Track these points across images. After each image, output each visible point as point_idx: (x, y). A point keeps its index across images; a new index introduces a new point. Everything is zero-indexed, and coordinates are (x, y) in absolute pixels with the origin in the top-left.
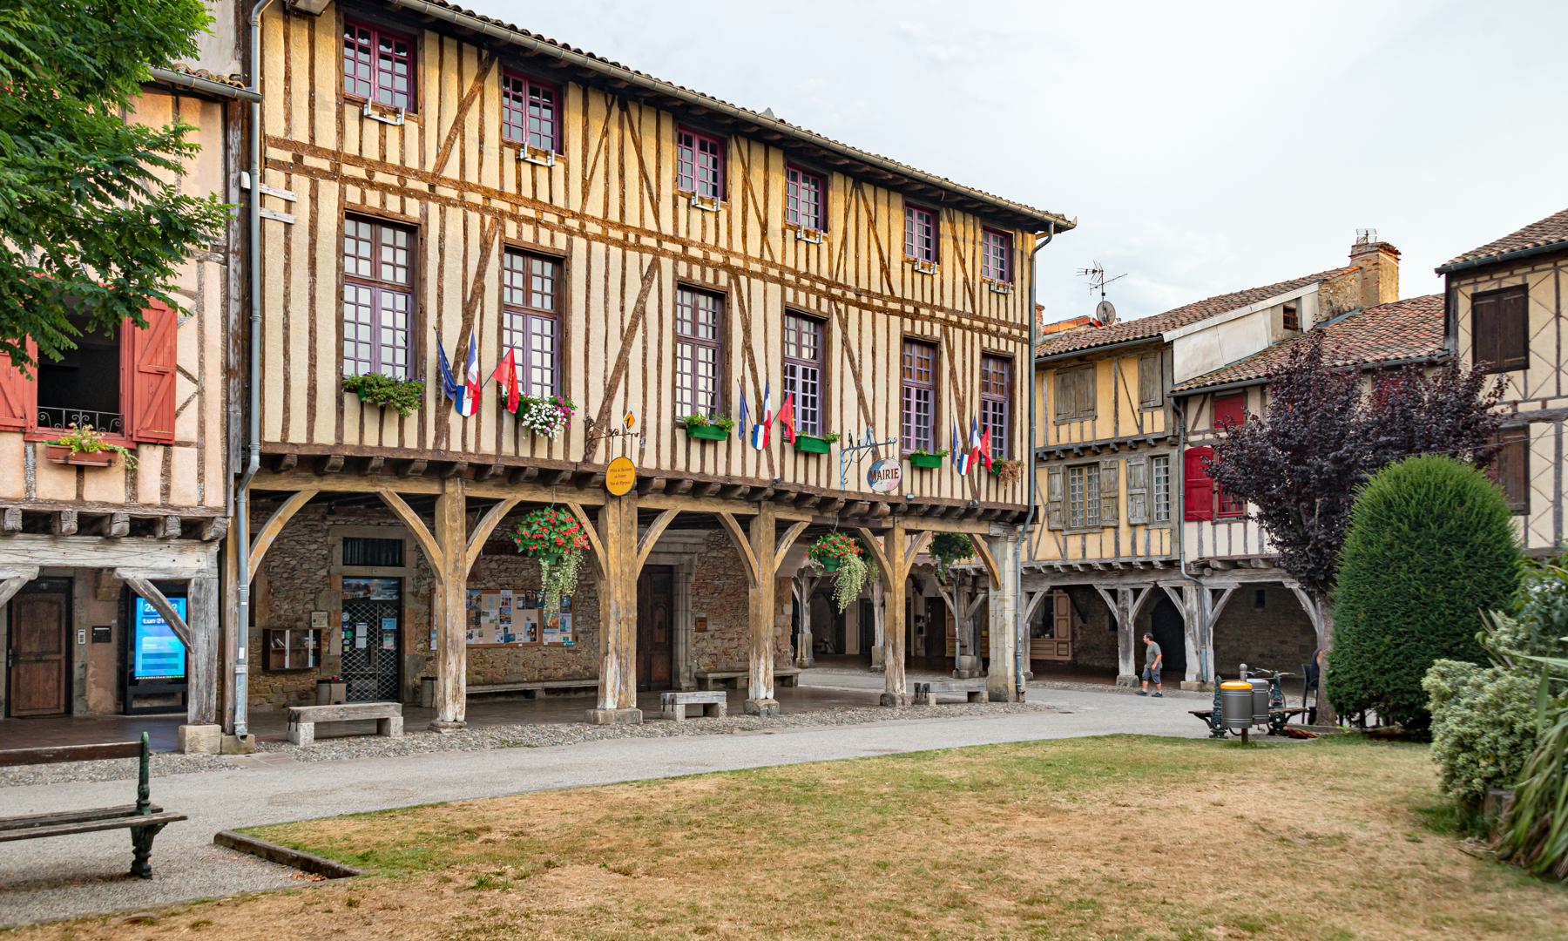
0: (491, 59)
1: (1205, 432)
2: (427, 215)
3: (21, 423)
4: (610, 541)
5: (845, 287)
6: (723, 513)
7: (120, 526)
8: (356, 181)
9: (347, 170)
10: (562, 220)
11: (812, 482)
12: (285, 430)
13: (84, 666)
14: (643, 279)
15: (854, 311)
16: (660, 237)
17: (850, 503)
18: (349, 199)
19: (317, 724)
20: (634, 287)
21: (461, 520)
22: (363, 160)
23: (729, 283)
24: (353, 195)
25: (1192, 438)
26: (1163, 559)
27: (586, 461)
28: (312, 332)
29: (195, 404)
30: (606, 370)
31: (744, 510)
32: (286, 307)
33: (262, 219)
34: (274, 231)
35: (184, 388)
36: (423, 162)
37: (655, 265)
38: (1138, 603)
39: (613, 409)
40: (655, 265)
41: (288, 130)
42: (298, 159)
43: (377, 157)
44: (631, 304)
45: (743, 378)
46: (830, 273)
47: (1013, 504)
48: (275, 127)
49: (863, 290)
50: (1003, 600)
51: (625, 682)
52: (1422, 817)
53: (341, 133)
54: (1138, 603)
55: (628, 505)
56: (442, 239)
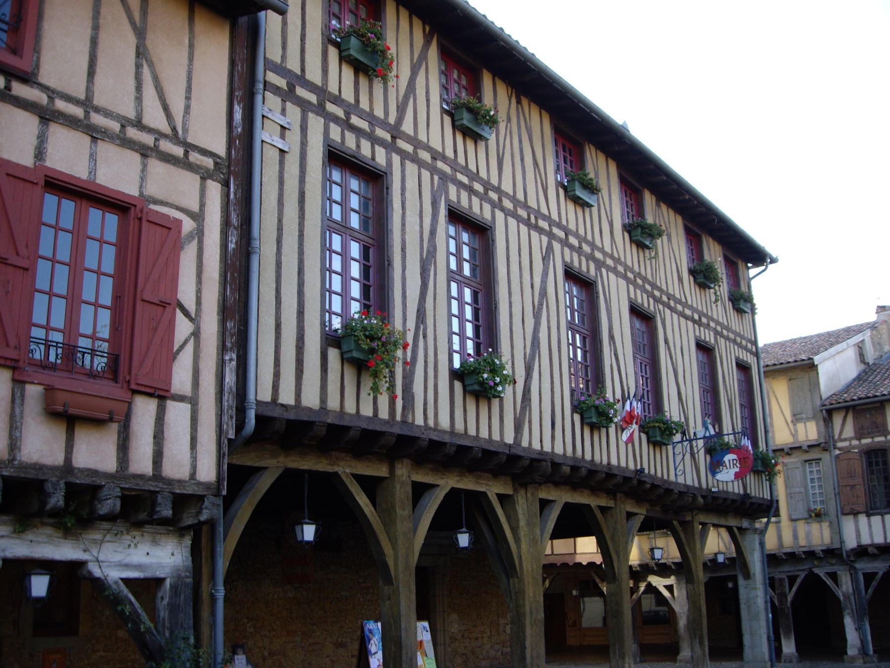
1: (850, 439)
3: (12, 354)
6: (593, 506)
7: (110, 504)
8: (336, 119)
9: (330, 107)
14: (543, 259)
22: (343, 101)
24: (335, 132)
25: (840, 444)
26: (824, 548)
29: (190, 347)
30: (525, 347)
31: (604, 502)
35: (183, 327)
36: (386, 113)
37: (550, 248)
38: (794, 589)
40: (550, 248)
41: (284, 57)
42: (291, 88)
45: (611, 365)
50: (755, 589)
54: (794, 589)
55: (532, 494)
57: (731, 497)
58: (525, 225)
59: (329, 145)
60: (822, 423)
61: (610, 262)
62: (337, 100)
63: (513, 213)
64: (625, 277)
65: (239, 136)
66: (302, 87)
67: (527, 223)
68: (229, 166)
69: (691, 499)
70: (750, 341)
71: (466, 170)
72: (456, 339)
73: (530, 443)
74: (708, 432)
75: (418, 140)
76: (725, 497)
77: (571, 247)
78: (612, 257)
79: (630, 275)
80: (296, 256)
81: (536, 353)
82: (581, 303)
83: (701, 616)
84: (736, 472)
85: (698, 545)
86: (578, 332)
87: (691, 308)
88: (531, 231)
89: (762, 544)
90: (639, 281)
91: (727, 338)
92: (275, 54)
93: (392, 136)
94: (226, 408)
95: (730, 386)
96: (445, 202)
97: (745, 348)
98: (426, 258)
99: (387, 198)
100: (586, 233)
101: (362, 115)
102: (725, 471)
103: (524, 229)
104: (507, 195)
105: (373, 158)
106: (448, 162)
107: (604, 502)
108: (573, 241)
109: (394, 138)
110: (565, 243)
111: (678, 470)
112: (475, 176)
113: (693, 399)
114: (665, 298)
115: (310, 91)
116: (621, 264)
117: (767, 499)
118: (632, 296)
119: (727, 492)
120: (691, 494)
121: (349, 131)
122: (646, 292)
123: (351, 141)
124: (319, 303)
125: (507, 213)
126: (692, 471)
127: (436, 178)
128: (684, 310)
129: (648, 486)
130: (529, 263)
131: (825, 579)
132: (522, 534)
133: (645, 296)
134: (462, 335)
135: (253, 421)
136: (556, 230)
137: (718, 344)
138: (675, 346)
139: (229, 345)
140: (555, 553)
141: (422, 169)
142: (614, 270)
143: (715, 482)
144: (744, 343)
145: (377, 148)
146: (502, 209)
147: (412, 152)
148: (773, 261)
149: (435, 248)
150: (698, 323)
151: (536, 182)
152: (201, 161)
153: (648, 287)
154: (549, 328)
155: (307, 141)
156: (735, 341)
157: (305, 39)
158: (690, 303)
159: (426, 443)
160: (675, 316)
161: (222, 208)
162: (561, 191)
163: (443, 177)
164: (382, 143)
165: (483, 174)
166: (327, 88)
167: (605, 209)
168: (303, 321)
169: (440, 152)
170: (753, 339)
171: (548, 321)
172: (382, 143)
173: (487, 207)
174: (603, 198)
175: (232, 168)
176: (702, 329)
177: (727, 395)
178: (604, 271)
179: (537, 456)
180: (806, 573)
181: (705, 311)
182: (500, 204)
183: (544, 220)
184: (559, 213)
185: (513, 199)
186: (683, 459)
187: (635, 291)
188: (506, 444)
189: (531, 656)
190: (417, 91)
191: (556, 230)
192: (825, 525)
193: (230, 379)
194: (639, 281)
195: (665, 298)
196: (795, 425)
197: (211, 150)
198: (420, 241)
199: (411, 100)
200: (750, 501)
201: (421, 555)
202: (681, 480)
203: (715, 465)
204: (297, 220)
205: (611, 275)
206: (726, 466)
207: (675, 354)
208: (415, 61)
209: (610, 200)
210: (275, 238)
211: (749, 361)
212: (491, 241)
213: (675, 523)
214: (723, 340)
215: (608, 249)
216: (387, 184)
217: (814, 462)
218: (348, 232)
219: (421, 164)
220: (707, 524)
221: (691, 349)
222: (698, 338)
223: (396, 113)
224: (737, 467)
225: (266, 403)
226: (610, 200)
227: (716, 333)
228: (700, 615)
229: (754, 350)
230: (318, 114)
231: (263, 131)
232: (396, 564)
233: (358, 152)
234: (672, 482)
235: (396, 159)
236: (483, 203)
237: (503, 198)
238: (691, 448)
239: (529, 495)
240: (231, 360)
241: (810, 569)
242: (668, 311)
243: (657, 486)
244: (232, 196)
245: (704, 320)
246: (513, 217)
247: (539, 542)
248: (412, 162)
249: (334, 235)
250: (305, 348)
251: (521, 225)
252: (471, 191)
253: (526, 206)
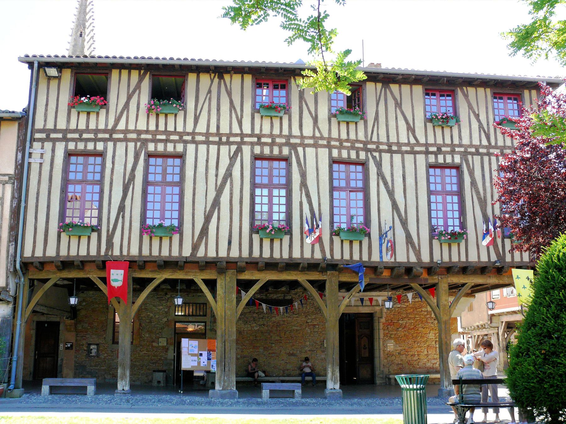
0: (145, 74)
4: (218, 298)
5: (378, 143)
10: (477, 150)
11: (356, 257)
13: (62, 360)
15: (386, 157)
16: (242, 135)
30: (205, 208)
34: (35, 168)
37: (239, 150)
39: (210, 227)
43: (478, 144)
44: (222, 171)
45: (301, 203)
46: (366, 136)
47: (324, 259)
48: (39, 124)
49: (392, 143)
56: (114, 157)
65: (19, 165)
98: (128, 183)
168: (48, 225)
208: (130, 93)
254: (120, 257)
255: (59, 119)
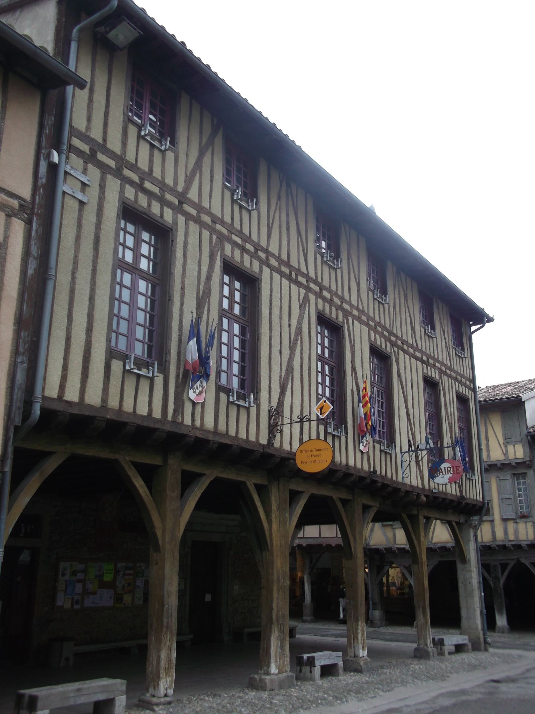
2: (186, 224)
6: (334, 497)
8: (132, 183)
9: (127, 172)
12: (62, 387)
14: (300, 306)
17: (407, 492)
18: (127, 195)
19: (51, 711)
20: (296, 310)
21: (177, 492)
22: (138, 169)
23: (344, 320)
24: (130, 193)
26: (529, 543)
27: (270, 443)
28: (92, 299)
30: (281, 372)
31: (344, 495)
32: (73, 273)
33: (64, 193)
36: (176, 182)
37: (306, 298)
40: (306, 298)
41: (88, 128)
44: (294, 322)
45: (352, 390)
51: (282, 647)
52: (157, 688)
53: (124, 143)
54: (506, 574)
57: (449, 497)
58: (287, 279)
59: (123, 202)
60: (527, 445)
61: (355, 312)
62: (134, 167)
63: (278, 269)
64: (367, 325)
66: (103, 153)
67: (289, 278)
68: (33, 209)
69: (415, 497)
70: (469, 380)
71: (240, 233)
72: (224, 362)
73: (281, 445)
74: (428, 445)
75: (202, 206)
76: (445, 497)
77: (324, 299)
78: (357, 309)
79: (371, 323)
80: (88, 285)
81: (289, 376)
82: (331, 342)
83: (424, 590)
84: (450, 477)
85: (422, 534)
86: (327, 364)
87: (421, 351)
88: (292, 284)
89: (476, 537)
90: (379, 329)
91: (450, 376)
92: (80, 123)
93: (179, 202)
94: (15, 400)
95: (451, 412)
96: (221, 256)
97: (465, 385)
98: (202, 297)
99: (172, 249)
100: (337, 289)
101: (154, 181)
102: (441, 475)
103: (285, 282)
104: (273, 255)
105: (162, 216)
106: (225, 226)
107: (344, 495)
108: (325, 294)
109: (181, 203)
110: (319, 295)
111: (405, 473)
112: (247, 239)
113: (420, 421)
114: (399, 343)
115: (110, 158)
116: (364, 315)
117: (480, 501)
118: (373, 338)
119: (446, 494)
120: (416, 493)
121: (141, 193)
122: (384, 336)
123: (143, 201)
124: (106, 324)
125: (272, 269)
126: (417, 475)
127: (214, 237)
128: (415, 353)
129: (379, 485)
130: (288, 308)
131: (530, 568)
132: (273, 516)
133: (383, 340)
134: (229, 359)
135: (38, 412)
136: (312, 285)
137: (442, 380)
138: (406, 379)
139: (21, 349)
140: (305, 536)
141: (203, 229)
142: (359, 319)
143: (436, 485)
144: (463, 380)
145: (166, 209)
146: (269, 266)
147: (195, 215)
148: (490, 320)
149: (210, 290)
150: (427, 363)
151: (298, 248)
152: (7, 201)
153: (386, 333)
154: (302, 358)
155: (104, 197)
156: (456, 379)
157: (108, 116)
158: (420, 348)
159: (192, 439)
160: (407, 357)
161: (24, 241)
162: (319, 257)
163: (221, 237)
164: (170, 205)
165: (255, 237)
166: (125, 156)
167: (354, 272)
169: (219, 218)
170: (471, 378)
171: (302, 353)
172: (170, 205)
173: (256, 264)
174: (353, 264)
175: (36, 211)
176: (429, 368)
177: (448, 419)
178: (350, 319)
179: (286, 455)
180: (515, 562)
181: (432, 355)
182: (267, 262)
183: (303, 277)
184: (316, 273)
185: (279, 259)
186: (409, 464)
187: (375, 336)
188: (261, 445)
189: (277, 615)
190: (203, 169)
191: (312, 285)
192: (530, 525)
193: (20, 377)
194: (379, 329)
195: (399, 343)
196: (506, 446)
197: (17, 193)
198: (198, 284)
199: (198, 175)
200: (465, 501)
201: (185, 530)
202: (407, 481)
203: (434, 471)
204: (91, 258)
205: (356, 323)
206: (442, 472)
207: (406, 385)
209: (359, 266)
210: (71, 269)
211: (467, 394)
212: (257, 289)
213: (404, 515)
214: (446, 378)
215: (354, 302)
216: (172, 238)
217: (521, 475)
218: (137, 272)
219: (202, 225)
220: (430, 518)
221: (419, 382)
222: (426, 375)
223: (184, 184)
224: (451, 473)
225: (53, 399)
226: (359, 266)
227: (441, 372)
228: (424, 590)
229: (472, 386)
230: (116, 176)
231: (65, 184)
232: (164, 536)
233: (148, 210)
234: (400, 483)
235: (181, 219)
236: (253, 259)
237: (270, 257)
238: (417, 457)
239: (281, 486)
240: (22, 362)
241: (518, 559)
242: (401, 353)
243: (387, 486)
244: (34, 233)
245: (431, 361)
246: (277, 273)
247: (288, 523)
248: (195, 223)
249: (125, 274)
250: (91, 358)
251: (283, 279)
252: (244, 250)
253: (288, 264)
254: (190, 429)
255: (110, 130)
